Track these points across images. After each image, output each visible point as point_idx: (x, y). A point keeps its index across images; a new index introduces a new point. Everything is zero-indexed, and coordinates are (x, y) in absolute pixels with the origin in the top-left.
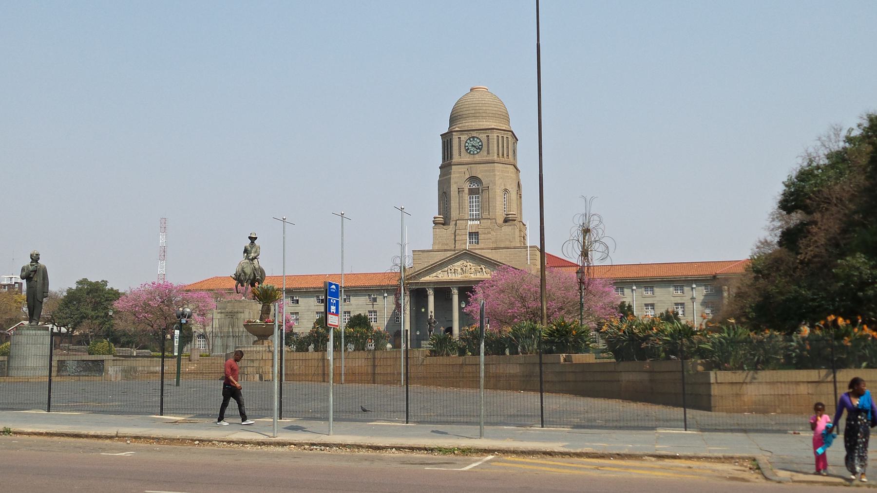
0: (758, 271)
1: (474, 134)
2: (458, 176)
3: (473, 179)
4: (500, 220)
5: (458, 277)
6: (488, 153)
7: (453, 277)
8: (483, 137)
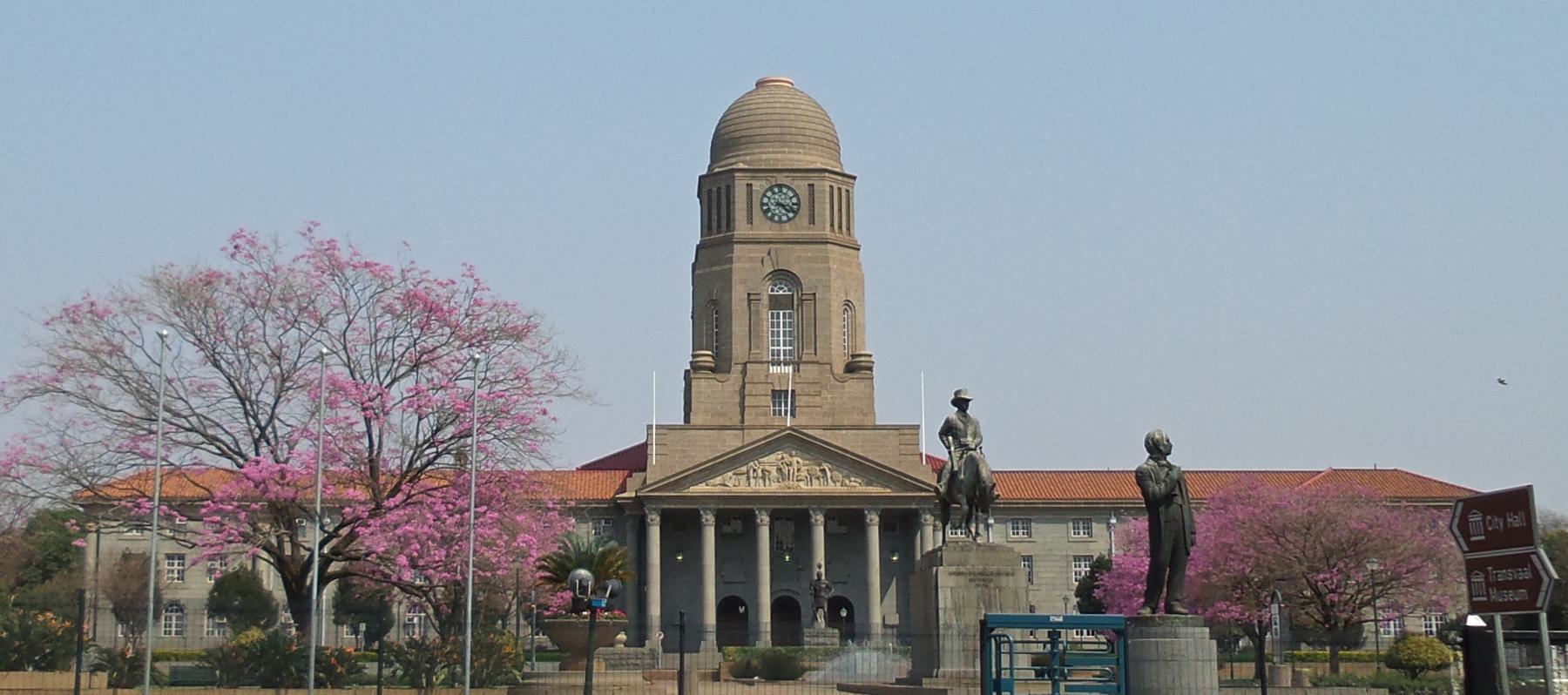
0: (1168, 498)
1: (782, 179)
2: (748, 270)
3: (782, 275)
4: (839, 368)
5: (773, 487)
6: (812, 221)
7: (758, 487)
8: (801, 186)
